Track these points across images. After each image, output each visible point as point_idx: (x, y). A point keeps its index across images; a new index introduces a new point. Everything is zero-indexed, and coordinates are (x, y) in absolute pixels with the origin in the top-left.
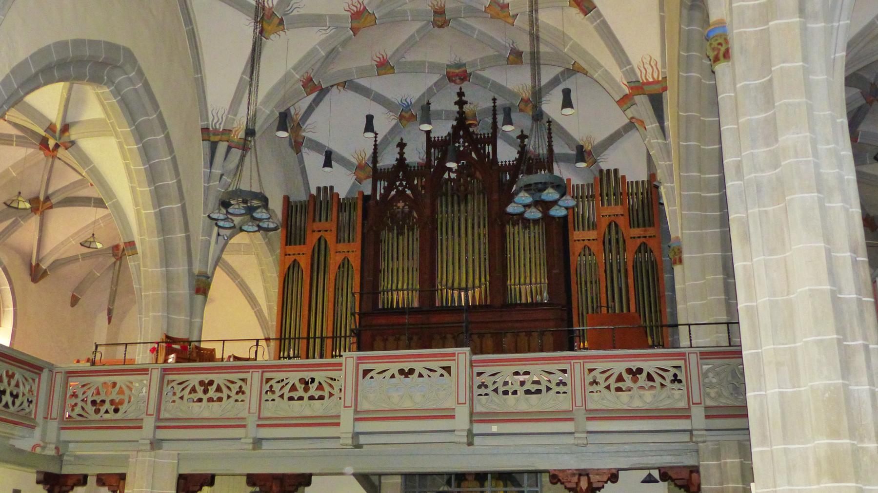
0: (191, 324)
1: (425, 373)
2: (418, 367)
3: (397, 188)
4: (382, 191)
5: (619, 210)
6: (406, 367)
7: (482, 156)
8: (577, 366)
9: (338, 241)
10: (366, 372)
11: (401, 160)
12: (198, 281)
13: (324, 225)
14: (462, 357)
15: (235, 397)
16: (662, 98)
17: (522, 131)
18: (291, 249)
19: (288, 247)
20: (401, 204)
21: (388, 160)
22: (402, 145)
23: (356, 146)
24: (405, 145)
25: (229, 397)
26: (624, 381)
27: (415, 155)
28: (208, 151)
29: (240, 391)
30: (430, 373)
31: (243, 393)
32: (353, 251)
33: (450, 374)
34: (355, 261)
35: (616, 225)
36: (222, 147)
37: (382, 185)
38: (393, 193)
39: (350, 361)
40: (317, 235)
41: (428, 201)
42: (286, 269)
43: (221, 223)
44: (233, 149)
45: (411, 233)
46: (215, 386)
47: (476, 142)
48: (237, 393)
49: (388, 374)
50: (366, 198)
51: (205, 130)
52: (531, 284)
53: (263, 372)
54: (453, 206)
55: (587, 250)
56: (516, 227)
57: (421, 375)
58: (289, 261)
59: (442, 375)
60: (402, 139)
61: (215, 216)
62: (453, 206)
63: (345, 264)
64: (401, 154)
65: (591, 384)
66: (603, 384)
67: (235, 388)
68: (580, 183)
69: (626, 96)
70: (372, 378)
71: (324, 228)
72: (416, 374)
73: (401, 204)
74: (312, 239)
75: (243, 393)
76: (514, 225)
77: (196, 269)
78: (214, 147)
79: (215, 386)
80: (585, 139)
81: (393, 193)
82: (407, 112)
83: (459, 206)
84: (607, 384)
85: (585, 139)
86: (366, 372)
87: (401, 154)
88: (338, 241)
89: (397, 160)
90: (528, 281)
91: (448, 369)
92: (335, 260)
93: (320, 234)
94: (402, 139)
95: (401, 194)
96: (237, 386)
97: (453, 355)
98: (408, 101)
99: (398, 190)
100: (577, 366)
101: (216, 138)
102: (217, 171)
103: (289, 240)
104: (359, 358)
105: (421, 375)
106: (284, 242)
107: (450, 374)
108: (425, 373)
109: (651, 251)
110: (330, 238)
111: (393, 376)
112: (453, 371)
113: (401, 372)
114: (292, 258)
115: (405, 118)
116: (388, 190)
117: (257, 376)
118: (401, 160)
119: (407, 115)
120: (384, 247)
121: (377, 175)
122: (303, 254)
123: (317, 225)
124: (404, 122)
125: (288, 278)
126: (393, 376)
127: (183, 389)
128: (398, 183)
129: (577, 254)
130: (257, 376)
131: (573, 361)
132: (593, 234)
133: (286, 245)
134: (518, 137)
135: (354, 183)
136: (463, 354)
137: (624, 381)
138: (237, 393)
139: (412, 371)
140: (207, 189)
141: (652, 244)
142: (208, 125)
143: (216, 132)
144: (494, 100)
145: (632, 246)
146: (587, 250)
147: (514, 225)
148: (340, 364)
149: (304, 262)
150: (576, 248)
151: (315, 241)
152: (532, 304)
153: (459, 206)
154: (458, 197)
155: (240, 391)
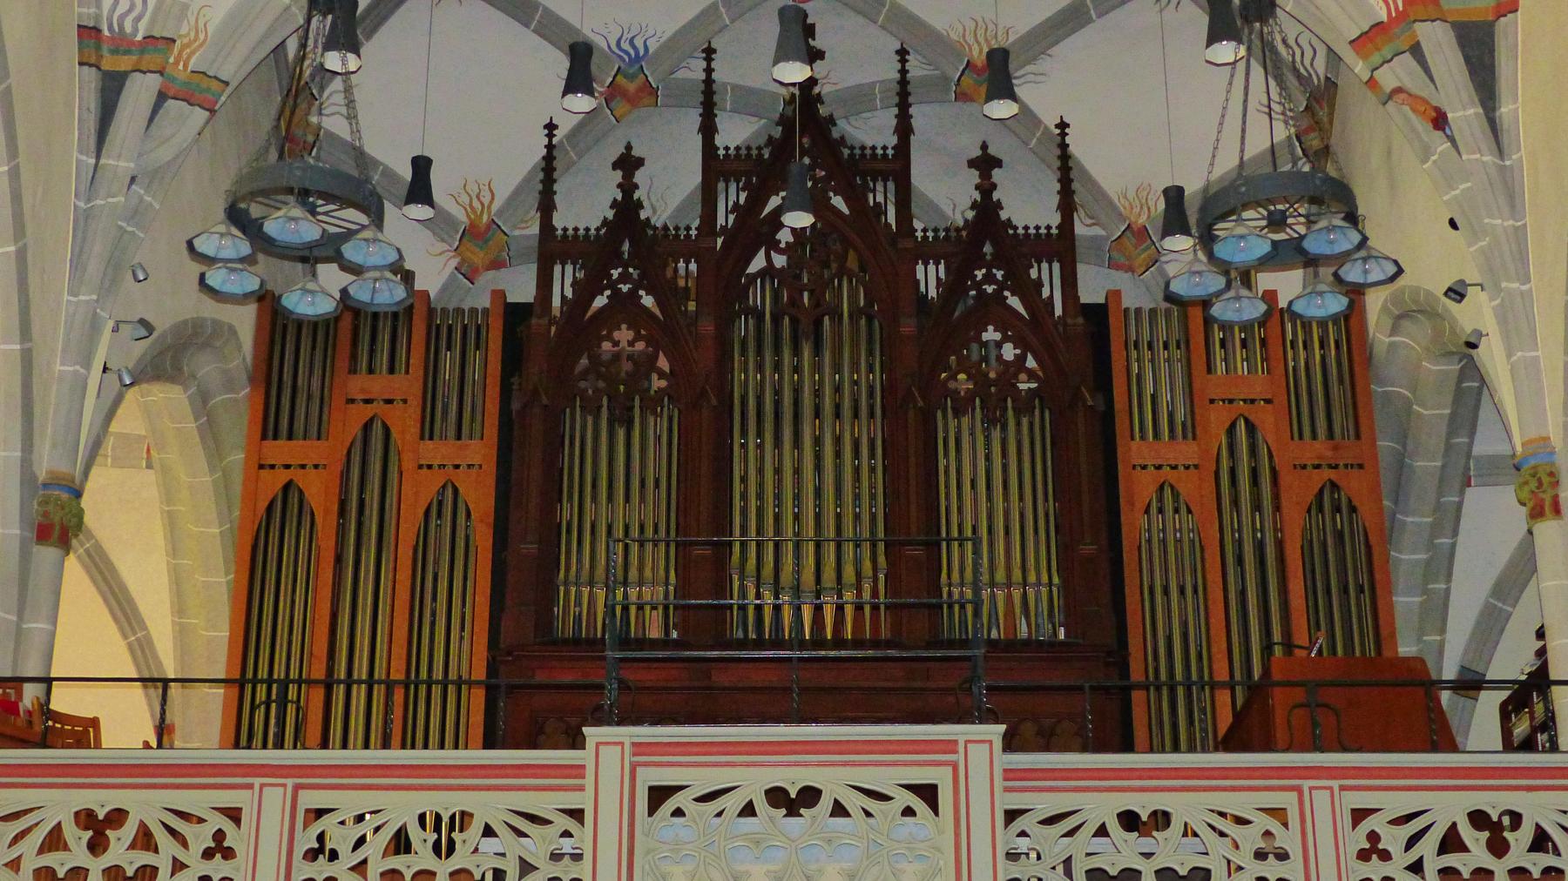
0: (19, 635)
1: (854, 802)
2: (833, 780)
3: (612, 285)
4: (569, 293)
5: (1259, 386)
6: (793, 779)
7: (868, 216)
8: (1322, 799)
9: (427, 431)
10: (659, 795)
11: (627, 207)
12: (45, 502)
13: (379, 385)
14: (978, 755)
15: (200, 867)
16: (1491, 35)
17: (984, 147)
18: (278, 451)
19: (269, 443)
20: (624, 334)
21: (585, 206)
22: (628, 163)
23: (486, 163)
24: (640, 162)
25: (178, 866)
26: (1465, 849)
27: (671, 190)
28: (93, 102)
29: (219, 848)
30: (872, 805)
31: (228, 854)
32: (472, 462)
33: (934, 807)
34: (479, 496)
35: (1251, 428)
36: (140, 92)
37: (564, 281)
38: (600, 301)
39: (610, 756)
40: (359, 414)
41: (707, 327)
42: (262, 505)
43: (216, 278)
44: (170, 102)
45: (621, 434)
46: (129, 830)
47: (856, 170)
48: (208, 854)
49: (733, 803)
50: (515, 315)
51: (89, 33)
52: (1025, 584)
53: (297, 788)
54: (777, 350)
55: (1168, 492)
56: (965, 420)
57: (839, 810)
58: (273, 482)
59: (909, 812)
60: (629, 147)
61: (205, 245)
62: (777, 350)
63: (446, 503)
64: (628, 187)
65: (1364, 855)
66: (1401, 859)
67: (199, 838)
68: (1147, 305)
69: (1378, 26)
70: (678, 813)
71: (393, 391)
72: (825, 804)
73: (624, 334)
74: (345, 426)
75: (228, 854)
76: (957, 413)
77: (47, 462)
78: (111, 89)
79: (129, 830)
80: (1131, 195)
81: (600, 301)
82: (631, 78)
83: (796, 351)
84: (1412, 856)
85: (1131, 195)
86: (659, 795)
87: (628, 187)
88: (427, 431)
89: (614, 204)
90: (1000, 576)
91: (928, 793)
92: (415, 494)
93: (369, 411)
94: (629, 147)
95: (624, 307)
96: (208, 830)
97: (949, 746)
98: (639, 43)
99: (616, 293)
100: (1322, 799)
101: (124, 63)
102: (119, 161)
103: (272, 423)
104: (640, 748)
105: (839, 810)
106: (258, 435)
107: (934, 807)
108: (854, 802)
109: (1353, 509)
110: (404, 423)
111: (749, 810)
112: (945, 798)
113: (776, 796)
114: (283, 477)
115: (624, 94)
116: (585, 291)
117: (275, 798)
118: (627, 207)
119: (631, 87)
120: (569, 458)
121: (553, 248)
122: (315, 466)
123: (359, 384)
124: (621, 106)
125: (268, 544)
126: (749, 810)
127: (16, 839)
128: (615, 273)
129: (1140, 505)
130: (275, 798)
131: (1306, 784)
132: (1187, 452)
133: (264, 437)
134: (1057, 126)
135: (452, 278)
136: (980, 742)
137: (1465, 849)
138: (208, 854)
139: (810, 796)
140: (84, 220)
141: (1354, 485)
142: (98, 17)
143: (122, 44)
144: (902, 53)
145: (1299, 492)
146: (1168, 492)
147: (957, 413)
148: (578, 770)
149: (318, 491)
150: (1138, 488)
151: (356, 429)
152: (1027, 643)
153: (796, 351)
154: (795, 322)
155: (219, 848)
